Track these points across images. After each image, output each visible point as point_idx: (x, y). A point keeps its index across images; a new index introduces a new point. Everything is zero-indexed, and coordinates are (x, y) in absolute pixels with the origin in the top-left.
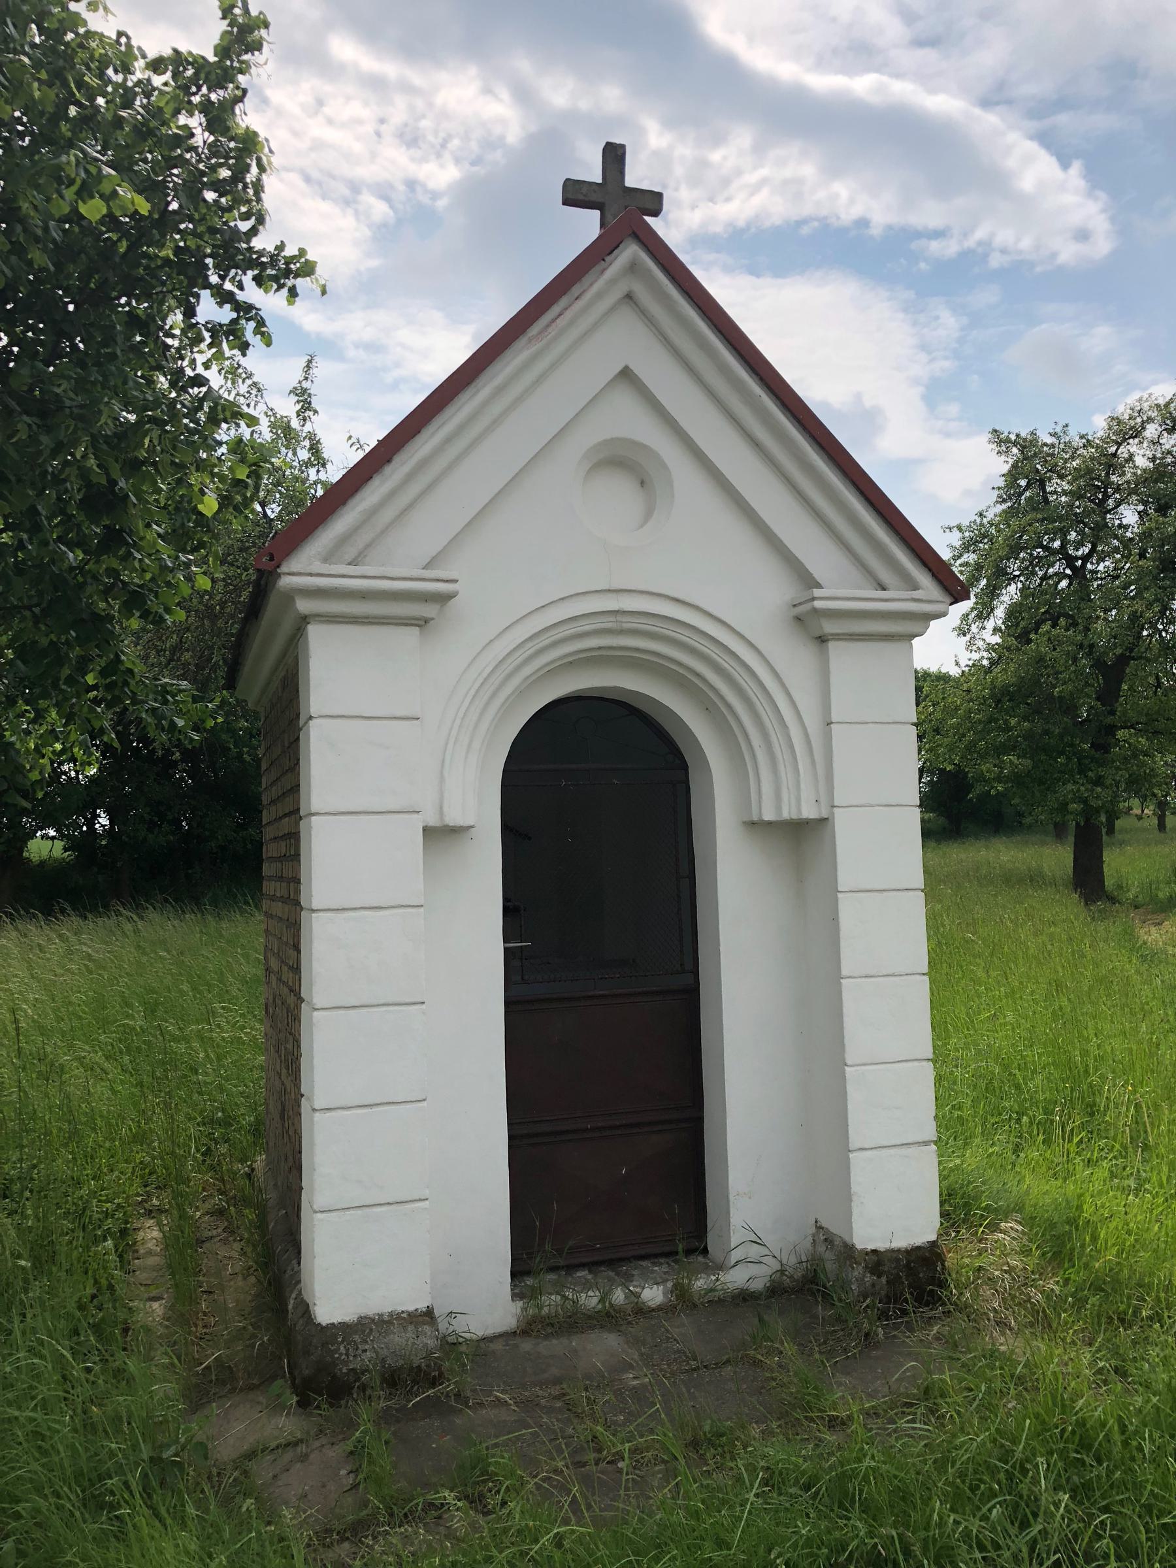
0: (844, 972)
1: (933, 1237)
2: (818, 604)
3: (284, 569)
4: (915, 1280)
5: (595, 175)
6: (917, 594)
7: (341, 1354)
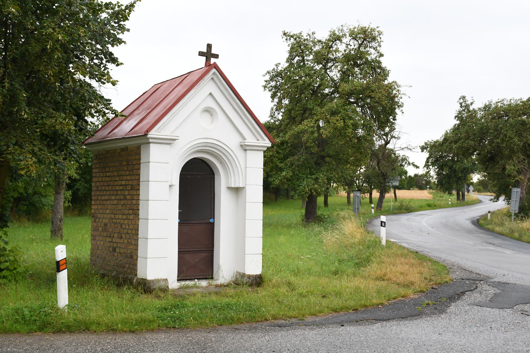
2: (246, 143)
4: (257, 281)
6: (265, 142)
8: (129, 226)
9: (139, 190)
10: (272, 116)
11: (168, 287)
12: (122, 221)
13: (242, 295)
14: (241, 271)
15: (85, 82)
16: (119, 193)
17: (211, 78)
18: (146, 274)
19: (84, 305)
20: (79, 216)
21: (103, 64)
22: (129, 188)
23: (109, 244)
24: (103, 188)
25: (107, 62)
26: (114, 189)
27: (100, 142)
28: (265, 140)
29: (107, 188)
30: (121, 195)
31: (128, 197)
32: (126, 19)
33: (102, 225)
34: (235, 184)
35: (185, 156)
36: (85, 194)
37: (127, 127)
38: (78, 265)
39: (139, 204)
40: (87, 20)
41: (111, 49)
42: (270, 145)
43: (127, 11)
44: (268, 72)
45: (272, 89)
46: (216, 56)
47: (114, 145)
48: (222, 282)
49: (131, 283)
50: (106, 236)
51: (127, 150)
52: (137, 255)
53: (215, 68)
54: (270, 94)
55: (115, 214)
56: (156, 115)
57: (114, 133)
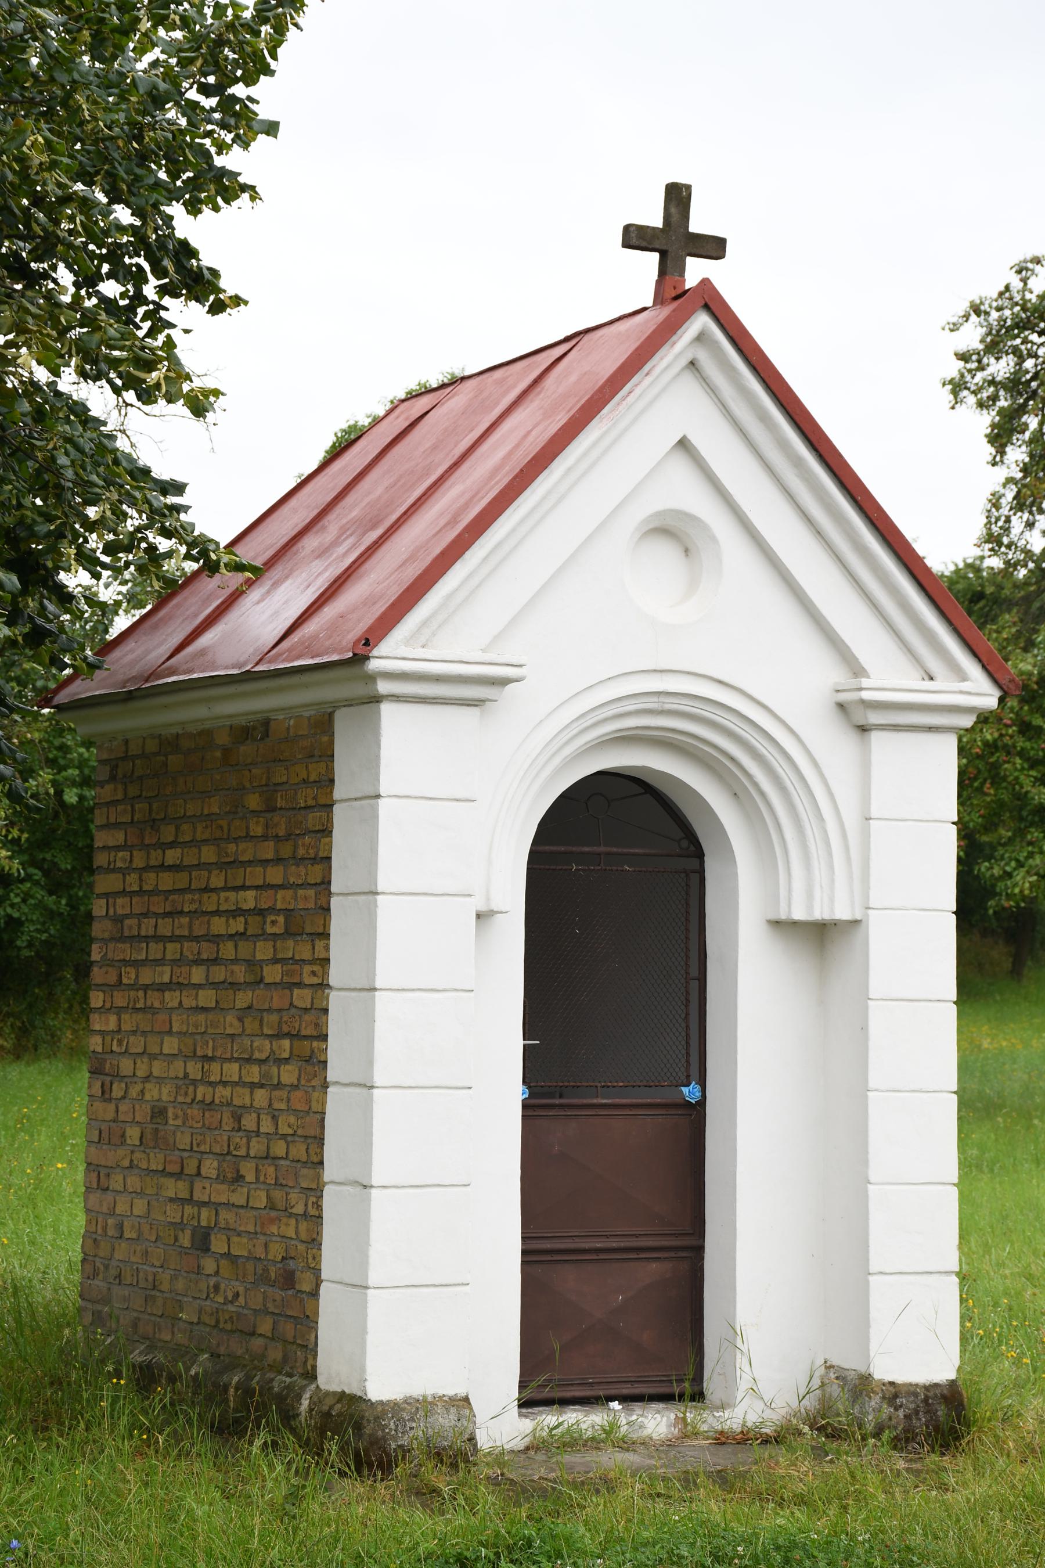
0: (871, 1085)
1: (952, 1375)
2: (866, 695)
3: (375, 652)
4: (938, 1420)
5: (656, 221)
6: (965, 686)
7: (391, 1430)
8: (274, 1118)
9: (325, 935)
10: (993, 540)
11: (472, 1439)
12: (242, 1097)
13: (861, 1497)
14: (850, 1362)
15: (58, 394)
16: (228, 950)
17: (684, 361)
18: (363, 1369)
19: (51, 1537)
20: (18, 1057)
21: (145, 301)
22: (277, 925)
23: (173, 1213)
24: (148, 927)
25: (162, 291)
26: (198, 931)
27: (129, 697)
28: (964, 677)
29: (165, 927)
30: (235, 961)
31: (273, 974)
32: (257, 68)
33: (143, 1113)
34: (810, 907)
35: (557, 760)
36: (48, 944)
37: (262, 619)
38: (18, 1321)
39: (326, 1011)
40: (62, 77)
41: (184, 225)
42: (989, 699)
43: (266, 29)
44: (977, 309)
45: (994, 398)
46: (714, 247)
47: (200, 712)
48: (752, 1419)
49: (288, 1417)
50: (163, 1172)
51: (266, 734)
52: (317, 1272)
53: (707, 307)
54: (985, 420)
55: (206, 1058)
56: (411, 558)
57: (203, 652)
